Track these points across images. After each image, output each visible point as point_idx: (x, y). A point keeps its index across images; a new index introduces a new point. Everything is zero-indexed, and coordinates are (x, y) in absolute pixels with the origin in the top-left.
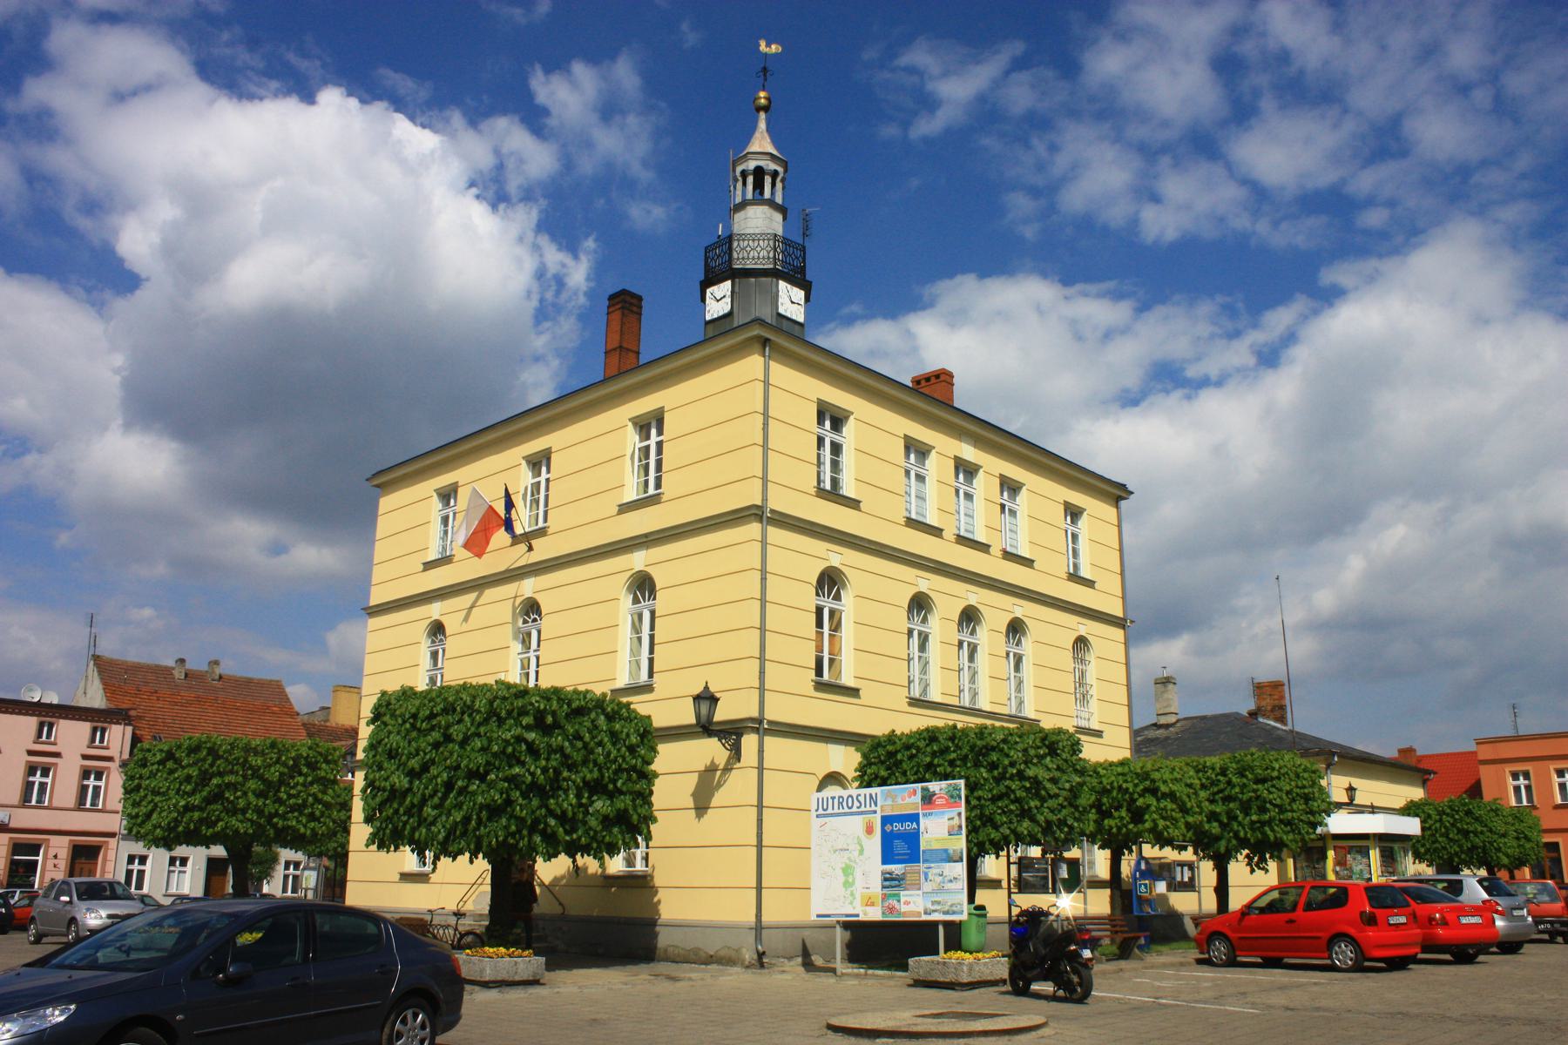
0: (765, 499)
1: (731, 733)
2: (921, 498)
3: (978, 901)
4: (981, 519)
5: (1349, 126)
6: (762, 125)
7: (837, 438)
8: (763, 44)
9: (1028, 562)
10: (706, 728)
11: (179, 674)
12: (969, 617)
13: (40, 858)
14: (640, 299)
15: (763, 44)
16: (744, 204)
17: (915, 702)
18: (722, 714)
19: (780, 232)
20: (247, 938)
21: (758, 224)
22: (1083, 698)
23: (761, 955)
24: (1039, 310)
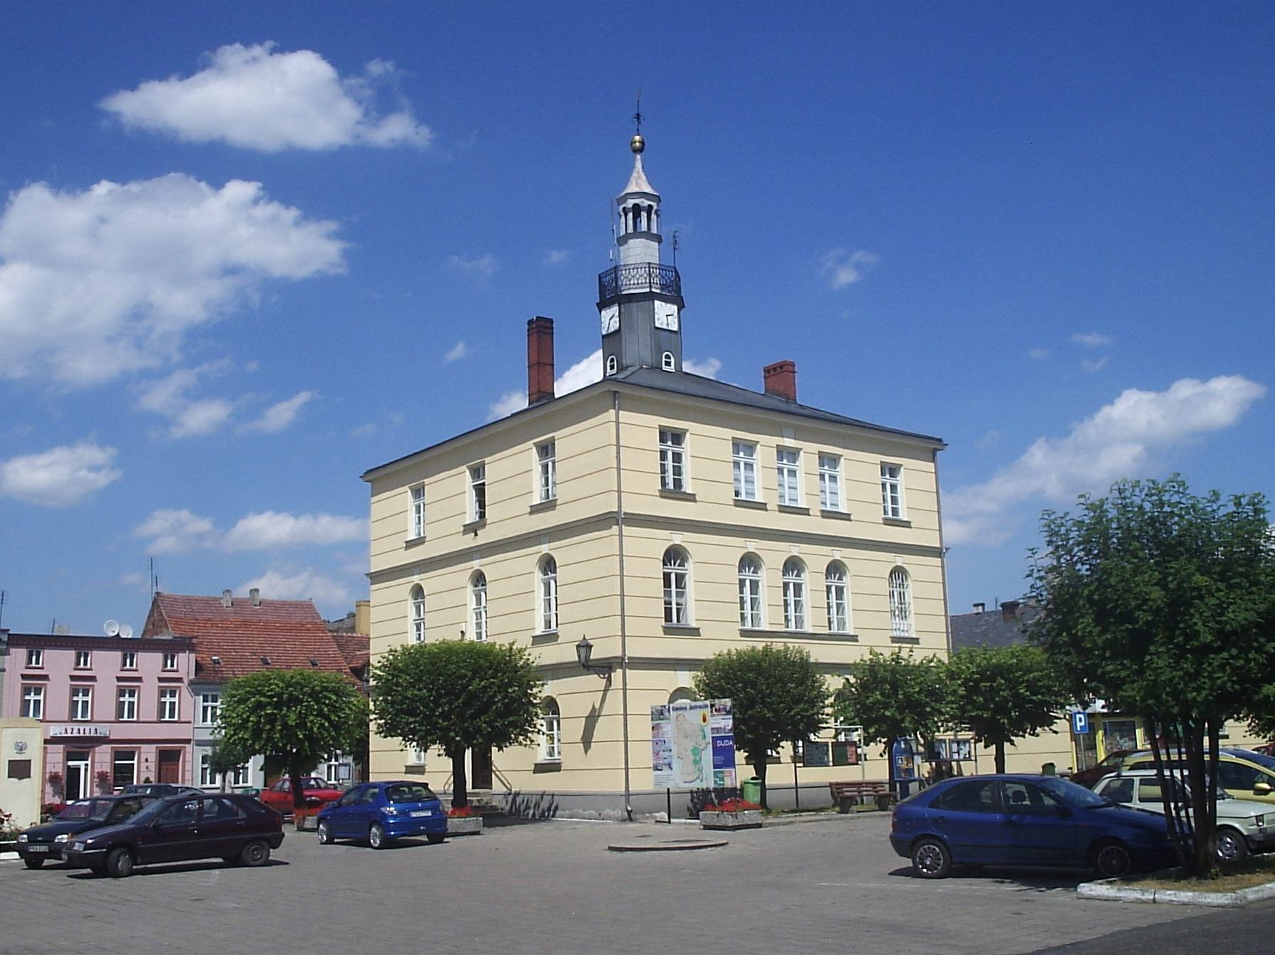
0: (620, 506)
1: (605, 667)
2: (749, 481)
4: (804, 488)
6: (639, 165)
7: (677, 450)
9: (846, 517)
11: (226, 602)
12: (793, 565)
13: (135, 762)
16: (628, 237)
17: (745, 633)
18: (594, 655)
20: (1048, 801)
22: (903, 614)
23: (629, 812)
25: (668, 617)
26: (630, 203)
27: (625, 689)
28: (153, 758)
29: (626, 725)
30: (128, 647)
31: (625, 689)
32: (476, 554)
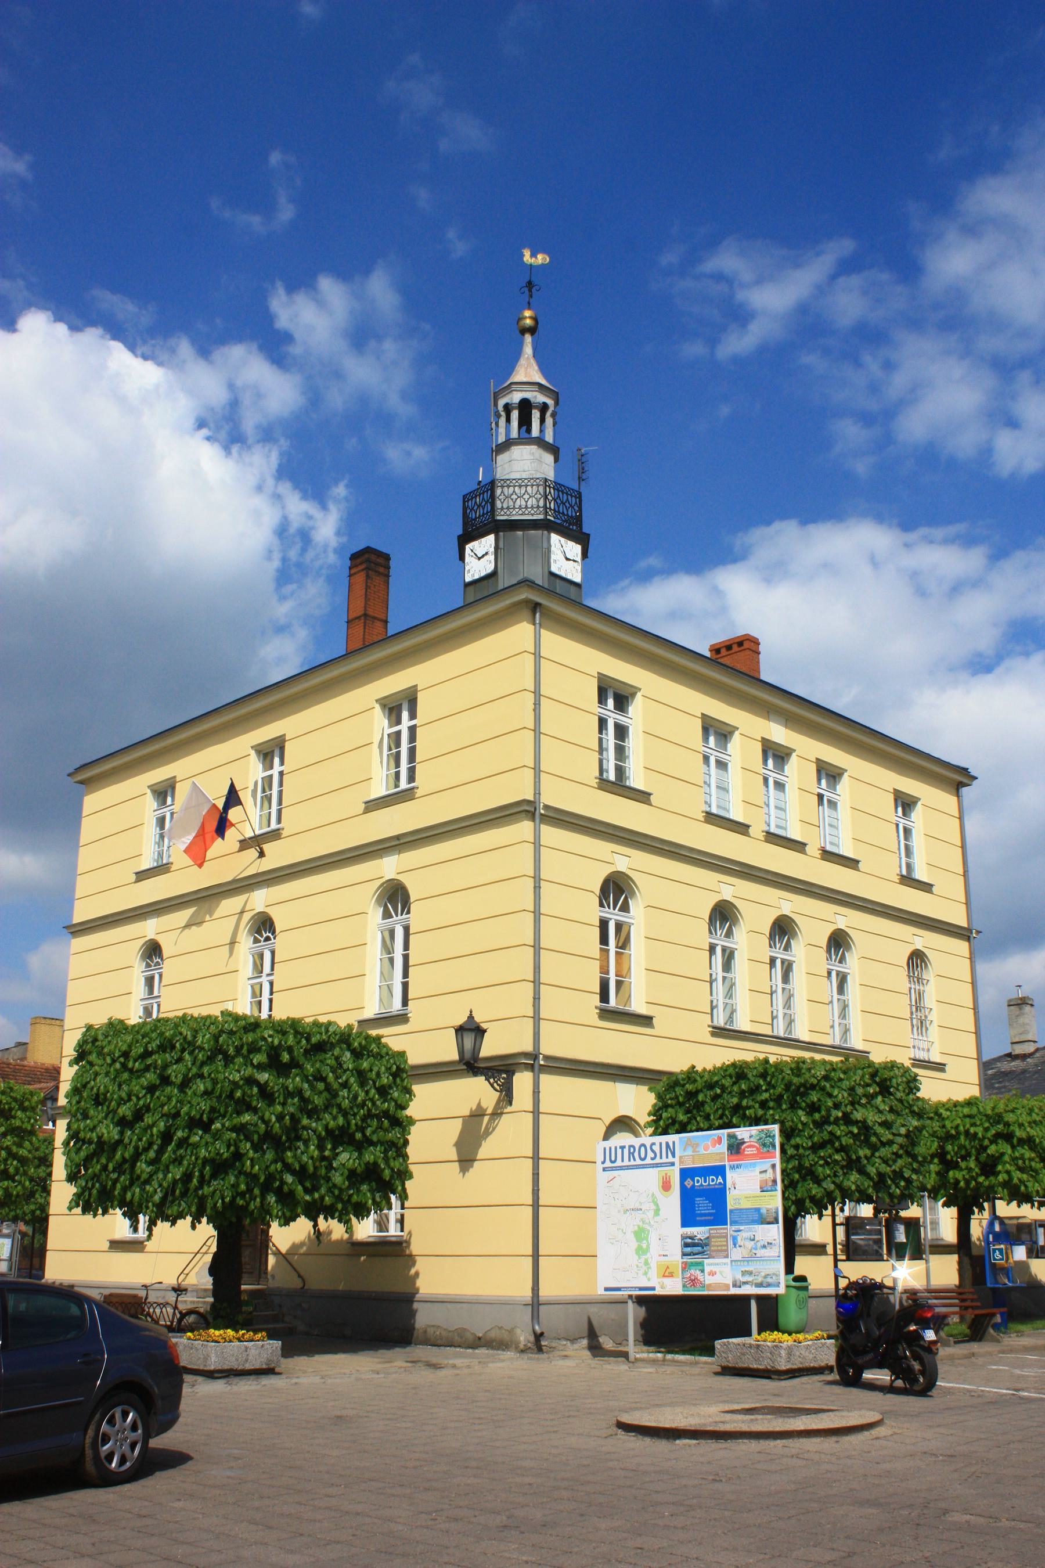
1: (500, 1071)
6: (528, 350)
7: (622, 719)
9: (852, 863)
10: (470, 1065)
17: (719, 1032)
18: (489, 1048)
22: (922, 1026)
25: (604, 996)
26: (516, 397)
27: (536, 1113)
29: (536, 1175)
31: (536, 1113)
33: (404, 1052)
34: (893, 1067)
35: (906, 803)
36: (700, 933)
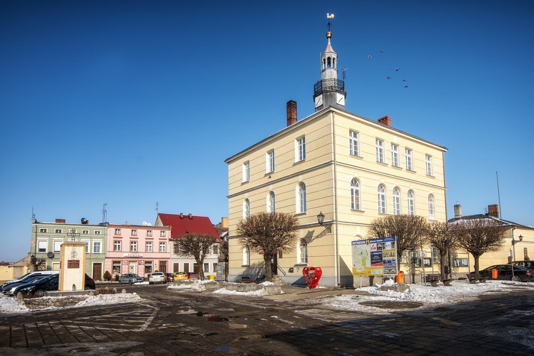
3: (401, 270)
5: (233, 232)
6: (329, 43)
7: (356, 139)
8: (328, 14)
10: (321, 224)
12: (397, 189)
14: (296, 103)
15: (328, 14)
19: (336, 78)
21: (331, 74)
24: (347, 282)
25: (353, 207)
28: (158, 264)
30: (149, 228)
32: (271, 181)
33: (489, 206)
34: (271, 220)
35: (429, 156)
36: (376, 191)
